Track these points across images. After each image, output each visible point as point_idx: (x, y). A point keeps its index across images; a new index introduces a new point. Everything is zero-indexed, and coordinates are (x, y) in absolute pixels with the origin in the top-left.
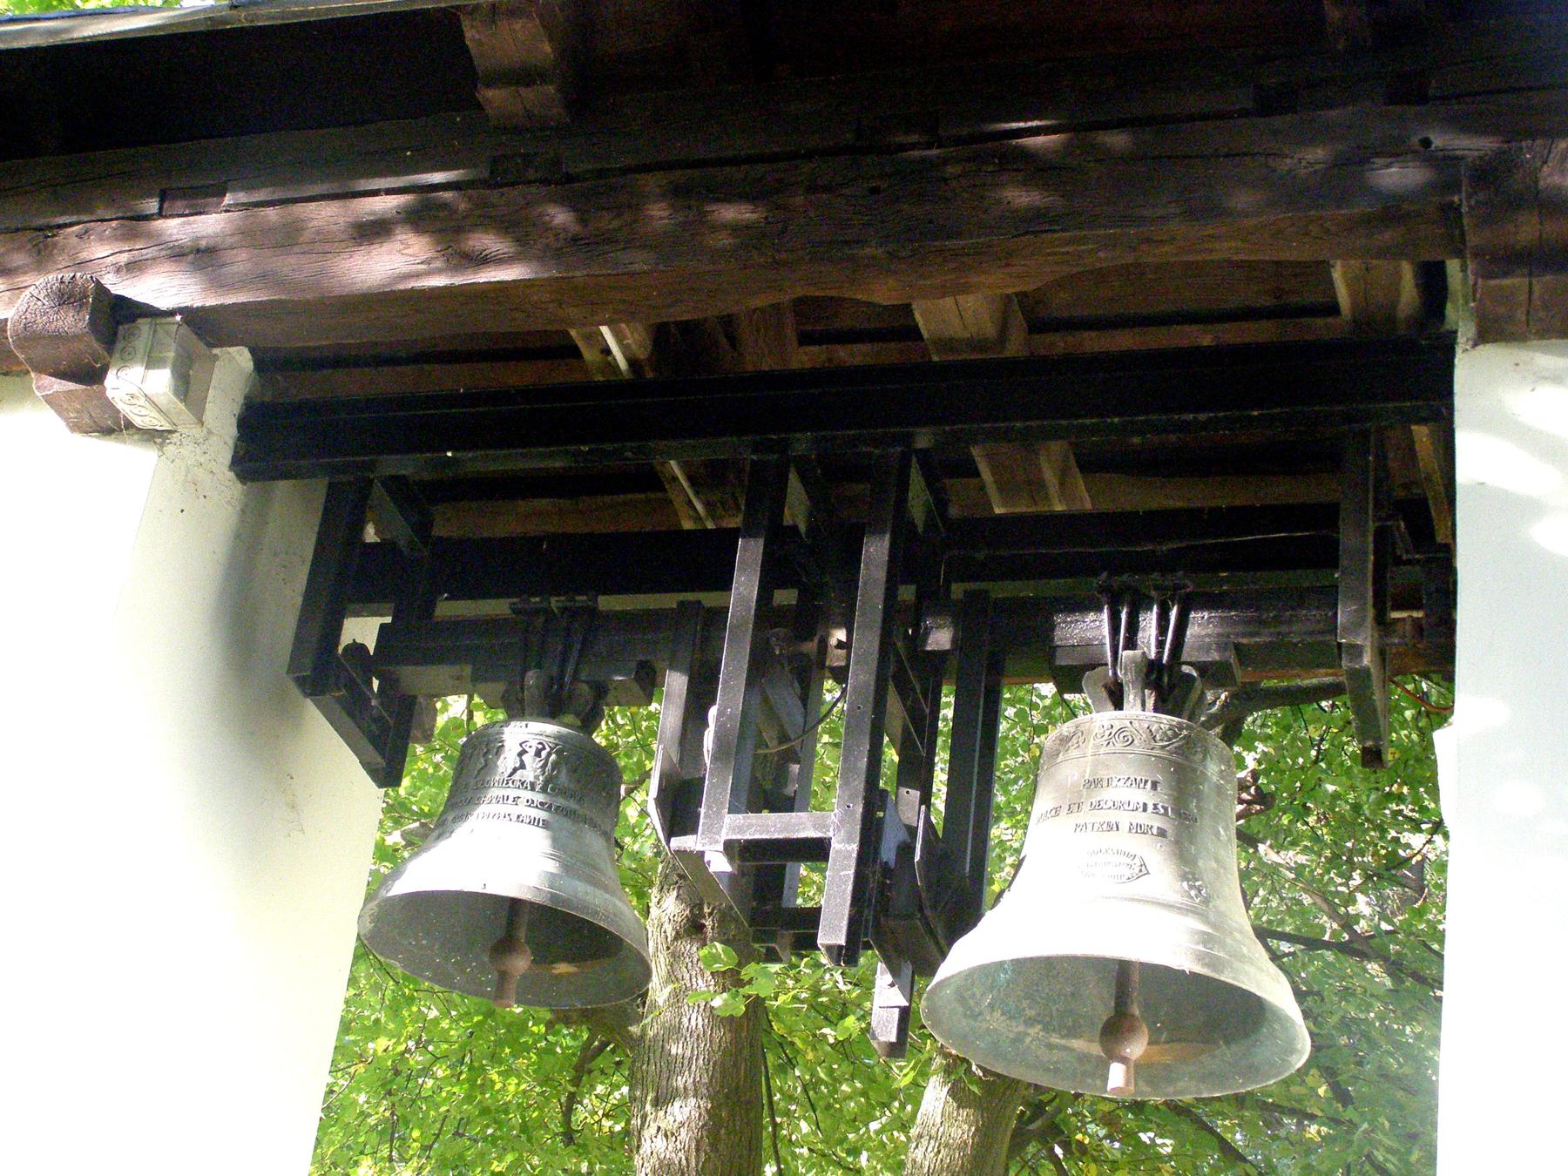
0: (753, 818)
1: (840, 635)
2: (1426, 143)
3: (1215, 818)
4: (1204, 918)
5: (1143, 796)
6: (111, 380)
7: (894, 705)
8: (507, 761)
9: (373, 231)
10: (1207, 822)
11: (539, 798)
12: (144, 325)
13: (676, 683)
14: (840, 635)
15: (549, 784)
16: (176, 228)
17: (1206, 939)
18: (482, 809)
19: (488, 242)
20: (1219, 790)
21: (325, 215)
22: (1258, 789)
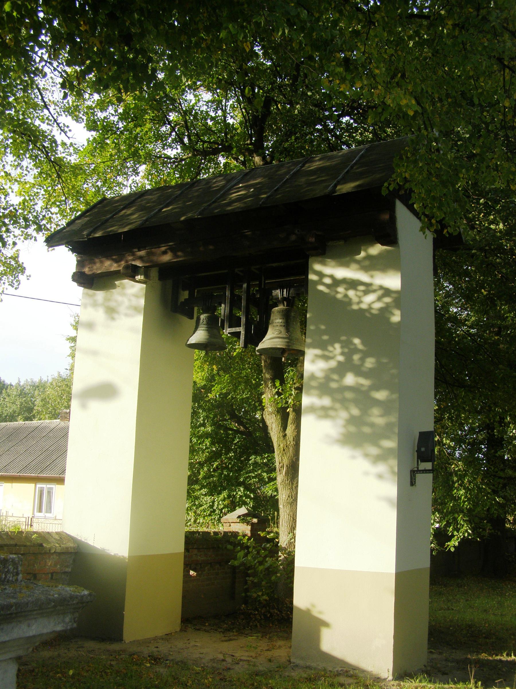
5: (280, 321)
9: (165, 253)
17: (288, 342)
19: (180, 254)
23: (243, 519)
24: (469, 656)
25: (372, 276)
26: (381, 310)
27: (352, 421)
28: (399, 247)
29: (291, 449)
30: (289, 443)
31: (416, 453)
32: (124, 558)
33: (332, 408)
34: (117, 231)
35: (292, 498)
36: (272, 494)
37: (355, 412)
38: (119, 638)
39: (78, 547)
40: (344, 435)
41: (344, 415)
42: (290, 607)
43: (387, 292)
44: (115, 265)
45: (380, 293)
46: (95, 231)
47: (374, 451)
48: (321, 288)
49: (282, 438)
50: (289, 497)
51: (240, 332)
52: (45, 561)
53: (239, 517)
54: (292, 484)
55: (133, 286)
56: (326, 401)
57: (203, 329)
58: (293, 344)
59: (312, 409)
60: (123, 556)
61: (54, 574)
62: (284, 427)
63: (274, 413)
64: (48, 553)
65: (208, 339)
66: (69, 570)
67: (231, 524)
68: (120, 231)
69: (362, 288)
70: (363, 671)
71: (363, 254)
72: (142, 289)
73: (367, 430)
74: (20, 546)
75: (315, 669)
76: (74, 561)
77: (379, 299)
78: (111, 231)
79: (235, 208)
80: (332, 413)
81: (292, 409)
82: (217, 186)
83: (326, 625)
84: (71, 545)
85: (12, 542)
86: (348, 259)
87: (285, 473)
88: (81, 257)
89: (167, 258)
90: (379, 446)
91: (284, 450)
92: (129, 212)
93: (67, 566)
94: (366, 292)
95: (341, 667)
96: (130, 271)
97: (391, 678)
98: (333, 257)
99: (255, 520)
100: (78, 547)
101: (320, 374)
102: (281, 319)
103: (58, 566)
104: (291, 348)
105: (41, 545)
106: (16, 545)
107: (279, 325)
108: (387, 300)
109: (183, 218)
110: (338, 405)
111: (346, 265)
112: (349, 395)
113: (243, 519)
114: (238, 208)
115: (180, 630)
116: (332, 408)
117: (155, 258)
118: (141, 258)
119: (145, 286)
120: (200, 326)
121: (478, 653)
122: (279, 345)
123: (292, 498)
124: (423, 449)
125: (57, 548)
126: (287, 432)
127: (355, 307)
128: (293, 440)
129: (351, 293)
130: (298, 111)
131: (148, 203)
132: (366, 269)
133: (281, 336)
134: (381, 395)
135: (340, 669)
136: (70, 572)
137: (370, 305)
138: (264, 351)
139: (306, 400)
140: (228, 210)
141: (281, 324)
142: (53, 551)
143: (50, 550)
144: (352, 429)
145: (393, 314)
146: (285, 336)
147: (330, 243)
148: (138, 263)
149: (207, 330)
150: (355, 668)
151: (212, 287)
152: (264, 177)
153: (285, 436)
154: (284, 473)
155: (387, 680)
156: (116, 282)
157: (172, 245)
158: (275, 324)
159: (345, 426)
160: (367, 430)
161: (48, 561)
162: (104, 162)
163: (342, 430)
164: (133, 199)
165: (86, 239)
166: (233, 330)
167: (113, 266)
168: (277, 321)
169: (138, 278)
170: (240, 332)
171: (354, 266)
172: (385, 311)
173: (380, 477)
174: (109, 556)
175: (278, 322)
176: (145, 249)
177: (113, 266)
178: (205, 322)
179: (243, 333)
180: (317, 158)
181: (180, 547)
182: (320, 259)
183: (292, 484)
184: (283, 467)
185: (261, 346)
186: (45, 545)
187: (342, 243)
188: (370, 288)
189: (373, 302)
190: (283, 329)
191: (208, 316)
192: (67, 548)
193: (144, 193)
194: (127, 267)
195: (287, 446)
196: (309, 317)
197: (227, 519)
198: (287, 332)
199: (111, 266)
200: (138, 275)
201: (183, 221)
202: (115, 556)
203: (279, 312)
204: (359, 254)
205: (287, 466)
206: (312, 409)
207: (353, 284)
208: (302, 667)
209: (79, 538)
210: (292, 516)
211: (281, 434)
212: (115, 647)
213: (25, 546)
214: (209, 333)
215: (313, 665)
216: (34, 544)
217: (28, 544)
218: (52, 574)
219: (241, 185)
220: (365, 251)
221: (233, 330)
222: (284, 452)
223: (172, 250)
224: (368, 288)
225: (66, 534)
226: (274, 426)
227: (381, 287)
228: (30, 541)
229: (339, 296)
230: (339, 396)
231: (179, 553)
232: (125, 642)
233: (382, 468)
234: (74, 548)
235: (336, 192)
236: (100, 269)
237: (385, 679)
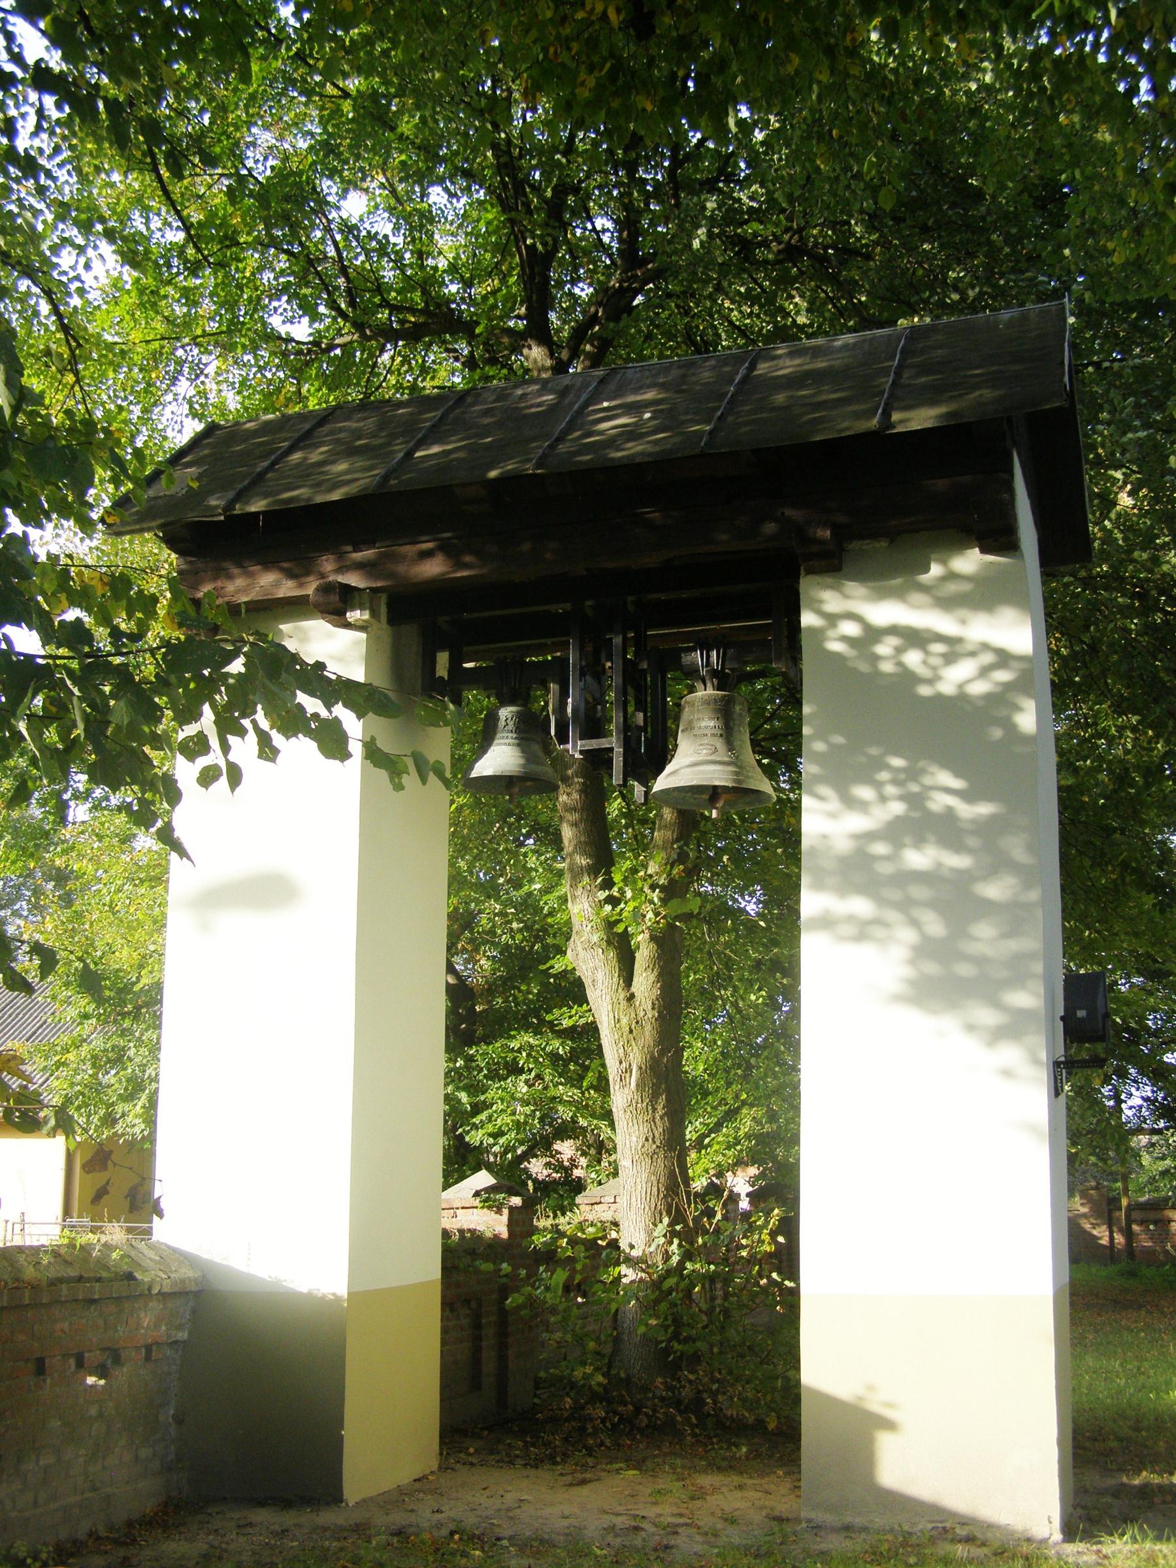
0: (588, 741)
1: (609, 664)
2: (783, 514)
3: (739, 725)
4: (737, 766)
5: (712, 724)
6: (348, 614)
7: (630, 690)
8: (502, 723)
9: (426, 555)
10: (736, 728)
11: (514, 736)
12: (356, 594)
13: (554, 687)
14: (609, 664)
15: (518, 730)
16: (358, 556)
17: (737, 774)
18: (496, 742)
19: (468, 559)
20: (740, 715)
21: (410, 550)
22: (580, 1088)
23: (486, 1197)
24: (1125, 1480)
25: (963, 622)
26: (988, 697)
27: (925, 949)
28: (1022, 556)
29: (648, 1027)
30: (642, 1014)
31: (1060, 1025)
32: (338, 1299)
33: (878, 922)
34: (309, 499)
35: (654, 1142)
36: (482, 1142)
37: (935, 926)
38: (334, 1497)
39: (204, 1276)
40: (912, 983)
41: (908, 935)
42: (791, 1392)
43: (1004, 658)
44: (290, 583)
45: (988, 658)
46: (241, 496)
47: (988, 1017)
48: (835, 646)
49: (624, 1003)
50: (647, 1139)
51: (611, 750)
52: (139, 1317)
53: (477, 1194)
54: (654, 1110)
55: (330, 636)
56: (861, 906)
57: (507, 741)
58: (749, 777)
59: (826, 922)
60: (334, 1294)
61: (154, 1348)
62: (627, 974)
63: (599, 946)
64: (146, 1294)
65: (524, 766)
66: (183, 1335)
67: (459, 1212)
68: (319, 499)
69: (938, 648)
70: (990, 1526)
71: (936, 570)
72: (357, 643)
73: (965, 970)
74: (89, 1280)
75: (865, 1529)
76: (194, 1311)
77: (984, 672)
78: (291, 500)
79: (632, 455)
80: (879, 932)
81: (647, 936)
82: (539, 405)
83: (889, 1425)
84: (187, 1273)
85: (73, 1273)
86: (898, 581)
87: (637, 1085)
88: (187, 562)
89: (434, 568)
90: (997, 1005)
91: (631, 1031)
92: (315, 456)
93: (179, 1327)
94: (950, 659)
95: (931, 1522)
96: (335, 598)
97: (1057, 1536)
98: (861, 576)
99: (516, 1201)
100: (204, 1276)
101: (843, 846)
102: (713, 719)
103: (163, 1328)
104: (744, 786)
105: (130, 1277)
106: (80, 1279)
107: (709, 732)
108: (1003, 676)
109: (493, 474)
110: (892, 916)
111: (899, 594)
112: (919, 892)
113: (486, 1197)
114: (638, 454)
115: (440, 1468)
116: (878, 922)
117: (401, 569)
118: (361, 566)
119: (363, 636)
120: (499, 735)
121: (1138, 1472)
122: (721, 779)
123: (654, 1142)
124: (1081, 1013)
125: (165, 1283)
126: (633, 989)
127: (924, 691)
128: (653, 1009)
129: (913, 659)
130: (701, 242)
131: (360, 438)
132: (947, 604)
133: (718, 759)
134: (994, 890)
135: (930, 1526)
136: (185, 1342)
137: (961, 686)
138: (672, 795)
139: (811, 902)
140: (613, 459)
141: (714, 731)
142: (155, 1291)
143: (149, 1289)
144: (931, 968)
145: (1018, 709)
146: (726, 759)
147: (855, 545)
148: (354, 580)
149: (518, 745)
150: (965, 1521)
151: (529, 642)
152: (663, 387)
153: (631, 998)
154: (633, 1084)
155: (1051, 1541)
156: (281, 627)
157: (449, 538)
158: (696, 732)
159: (912, 962)
160: (965, 970)
161: (142, 1315)
162: (148, 342)
163: (907, 971)
164: (307, 426)
165: (222, 518)
166: (593, 744)
167: (287, 589)
168: (703, 724)
169: (354, 616)
170: (611, 750)
171: (918, 597)
172: (1001, 700)
173: (1007, 1073)
174: (301, 1293)
175: (706, 727)
176: (374, 548)
177: (287, 589)
178: (511, 726)
179: (618, 751)
180: (780, 352)
181: (433, 1270)
182: (829, 580)
183: (654, 1110)
184: (629, 1070)
185: (661, 783)
186: (138, 1275)
187: (884, 544)
188: (959, 648)
189: (969, 681)
190: (719, 744)
191: (518, 712)
192: (183, 1281)
193: (331, 414)
194: (327, 589)
195: (637, 1022)
196: (810, 715)
197: (448, 1201)
198: (730, 750)
199: (277, 584)
200: (353, 610)
201: (496, 480)
202: (309, 1295)
203: (706, 702)
204: (927, 570)
205: (641, 1068)
206: (826, 922)
207: (915, 638)
208: (835, 1530)
209: (205, 1256)
210: (655, 1183)
211: (622, 995)
212: (328, 1517)
213: (99, 1280)
214: (523, 751)
215: (858, 1521)
216: (116, 1274)
217: (104, 1274)
218: (149, 1348)
219: (605, 404)
220: (944, 562)
221: (593, 744)
222: (631, 1036)
223: (447, 549)
224: (955, 649)
225: (169, 1247)
226: (600, 975)
227: (985, 647)
228: (107, 1268)
229: (887, 667)
230: (894, 894)
231: (423, 1285)
232: (347, 1505)
233: (1011, 1054)
234: (195, 1280)
235: (894, 427)
236: (245, 590)
237: (1044, 1541)
